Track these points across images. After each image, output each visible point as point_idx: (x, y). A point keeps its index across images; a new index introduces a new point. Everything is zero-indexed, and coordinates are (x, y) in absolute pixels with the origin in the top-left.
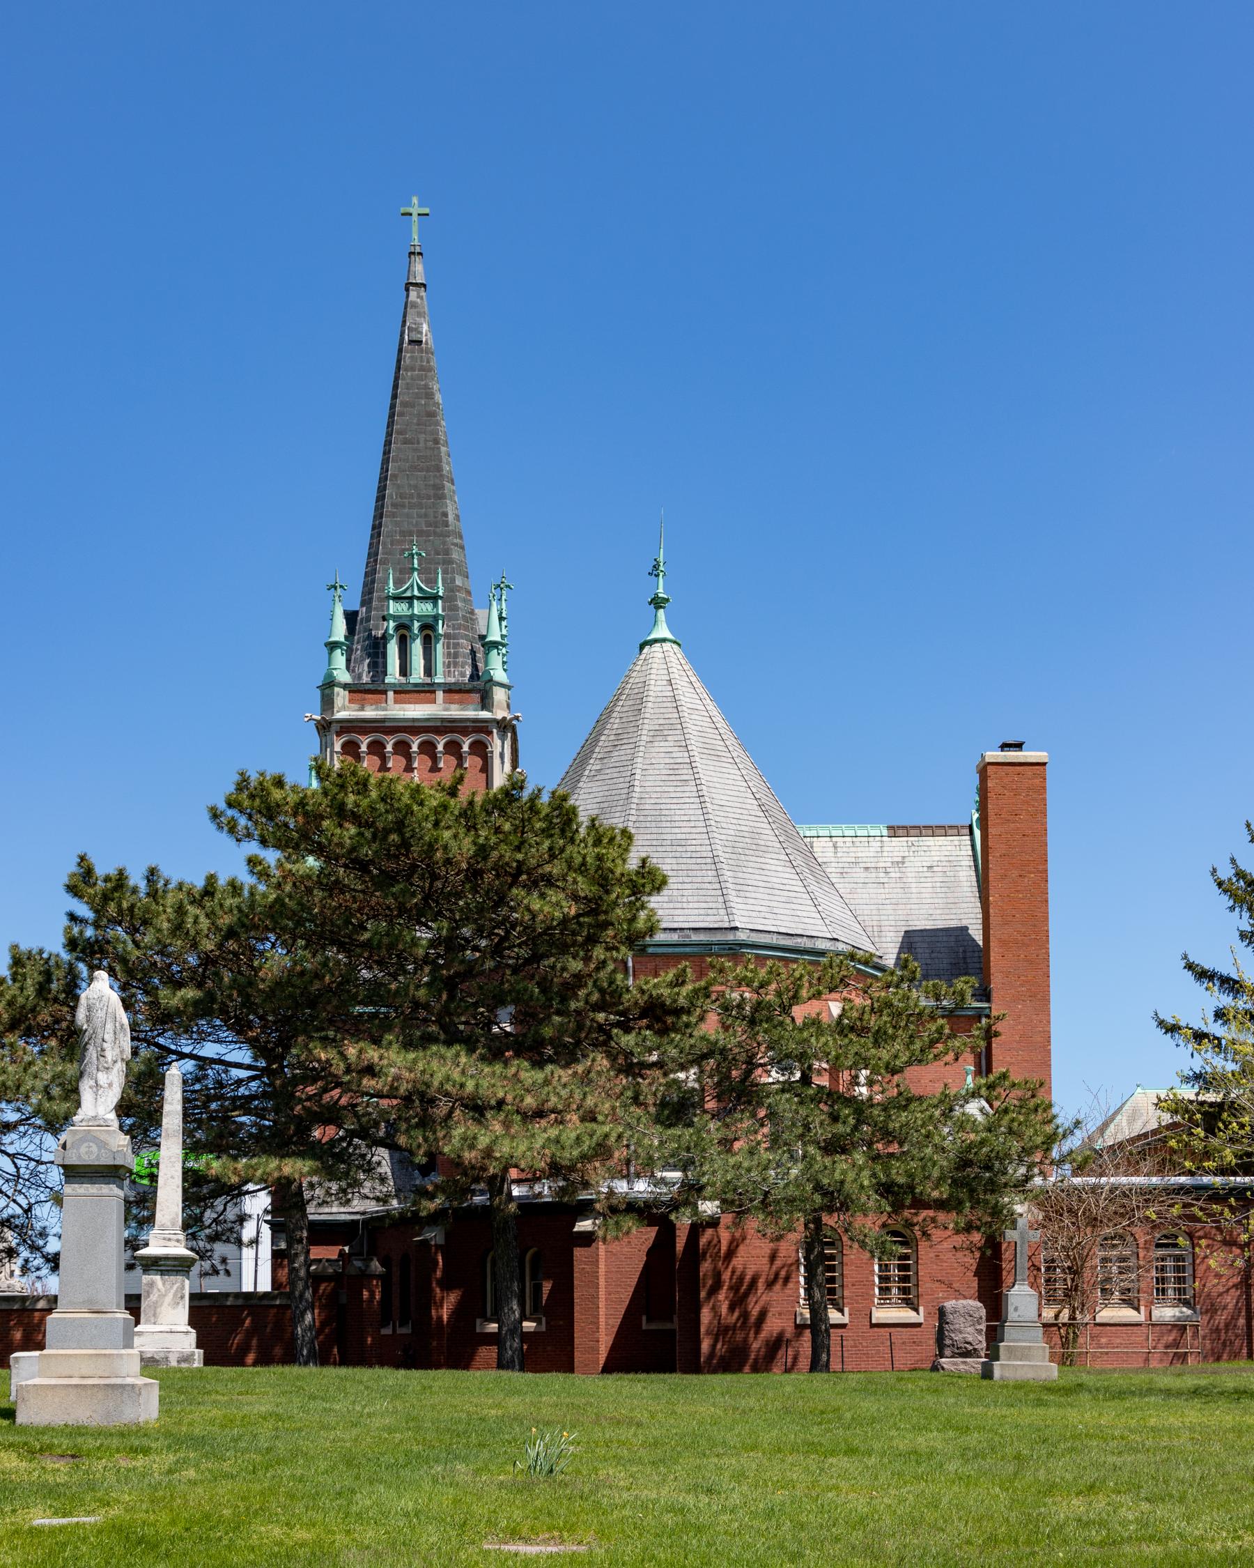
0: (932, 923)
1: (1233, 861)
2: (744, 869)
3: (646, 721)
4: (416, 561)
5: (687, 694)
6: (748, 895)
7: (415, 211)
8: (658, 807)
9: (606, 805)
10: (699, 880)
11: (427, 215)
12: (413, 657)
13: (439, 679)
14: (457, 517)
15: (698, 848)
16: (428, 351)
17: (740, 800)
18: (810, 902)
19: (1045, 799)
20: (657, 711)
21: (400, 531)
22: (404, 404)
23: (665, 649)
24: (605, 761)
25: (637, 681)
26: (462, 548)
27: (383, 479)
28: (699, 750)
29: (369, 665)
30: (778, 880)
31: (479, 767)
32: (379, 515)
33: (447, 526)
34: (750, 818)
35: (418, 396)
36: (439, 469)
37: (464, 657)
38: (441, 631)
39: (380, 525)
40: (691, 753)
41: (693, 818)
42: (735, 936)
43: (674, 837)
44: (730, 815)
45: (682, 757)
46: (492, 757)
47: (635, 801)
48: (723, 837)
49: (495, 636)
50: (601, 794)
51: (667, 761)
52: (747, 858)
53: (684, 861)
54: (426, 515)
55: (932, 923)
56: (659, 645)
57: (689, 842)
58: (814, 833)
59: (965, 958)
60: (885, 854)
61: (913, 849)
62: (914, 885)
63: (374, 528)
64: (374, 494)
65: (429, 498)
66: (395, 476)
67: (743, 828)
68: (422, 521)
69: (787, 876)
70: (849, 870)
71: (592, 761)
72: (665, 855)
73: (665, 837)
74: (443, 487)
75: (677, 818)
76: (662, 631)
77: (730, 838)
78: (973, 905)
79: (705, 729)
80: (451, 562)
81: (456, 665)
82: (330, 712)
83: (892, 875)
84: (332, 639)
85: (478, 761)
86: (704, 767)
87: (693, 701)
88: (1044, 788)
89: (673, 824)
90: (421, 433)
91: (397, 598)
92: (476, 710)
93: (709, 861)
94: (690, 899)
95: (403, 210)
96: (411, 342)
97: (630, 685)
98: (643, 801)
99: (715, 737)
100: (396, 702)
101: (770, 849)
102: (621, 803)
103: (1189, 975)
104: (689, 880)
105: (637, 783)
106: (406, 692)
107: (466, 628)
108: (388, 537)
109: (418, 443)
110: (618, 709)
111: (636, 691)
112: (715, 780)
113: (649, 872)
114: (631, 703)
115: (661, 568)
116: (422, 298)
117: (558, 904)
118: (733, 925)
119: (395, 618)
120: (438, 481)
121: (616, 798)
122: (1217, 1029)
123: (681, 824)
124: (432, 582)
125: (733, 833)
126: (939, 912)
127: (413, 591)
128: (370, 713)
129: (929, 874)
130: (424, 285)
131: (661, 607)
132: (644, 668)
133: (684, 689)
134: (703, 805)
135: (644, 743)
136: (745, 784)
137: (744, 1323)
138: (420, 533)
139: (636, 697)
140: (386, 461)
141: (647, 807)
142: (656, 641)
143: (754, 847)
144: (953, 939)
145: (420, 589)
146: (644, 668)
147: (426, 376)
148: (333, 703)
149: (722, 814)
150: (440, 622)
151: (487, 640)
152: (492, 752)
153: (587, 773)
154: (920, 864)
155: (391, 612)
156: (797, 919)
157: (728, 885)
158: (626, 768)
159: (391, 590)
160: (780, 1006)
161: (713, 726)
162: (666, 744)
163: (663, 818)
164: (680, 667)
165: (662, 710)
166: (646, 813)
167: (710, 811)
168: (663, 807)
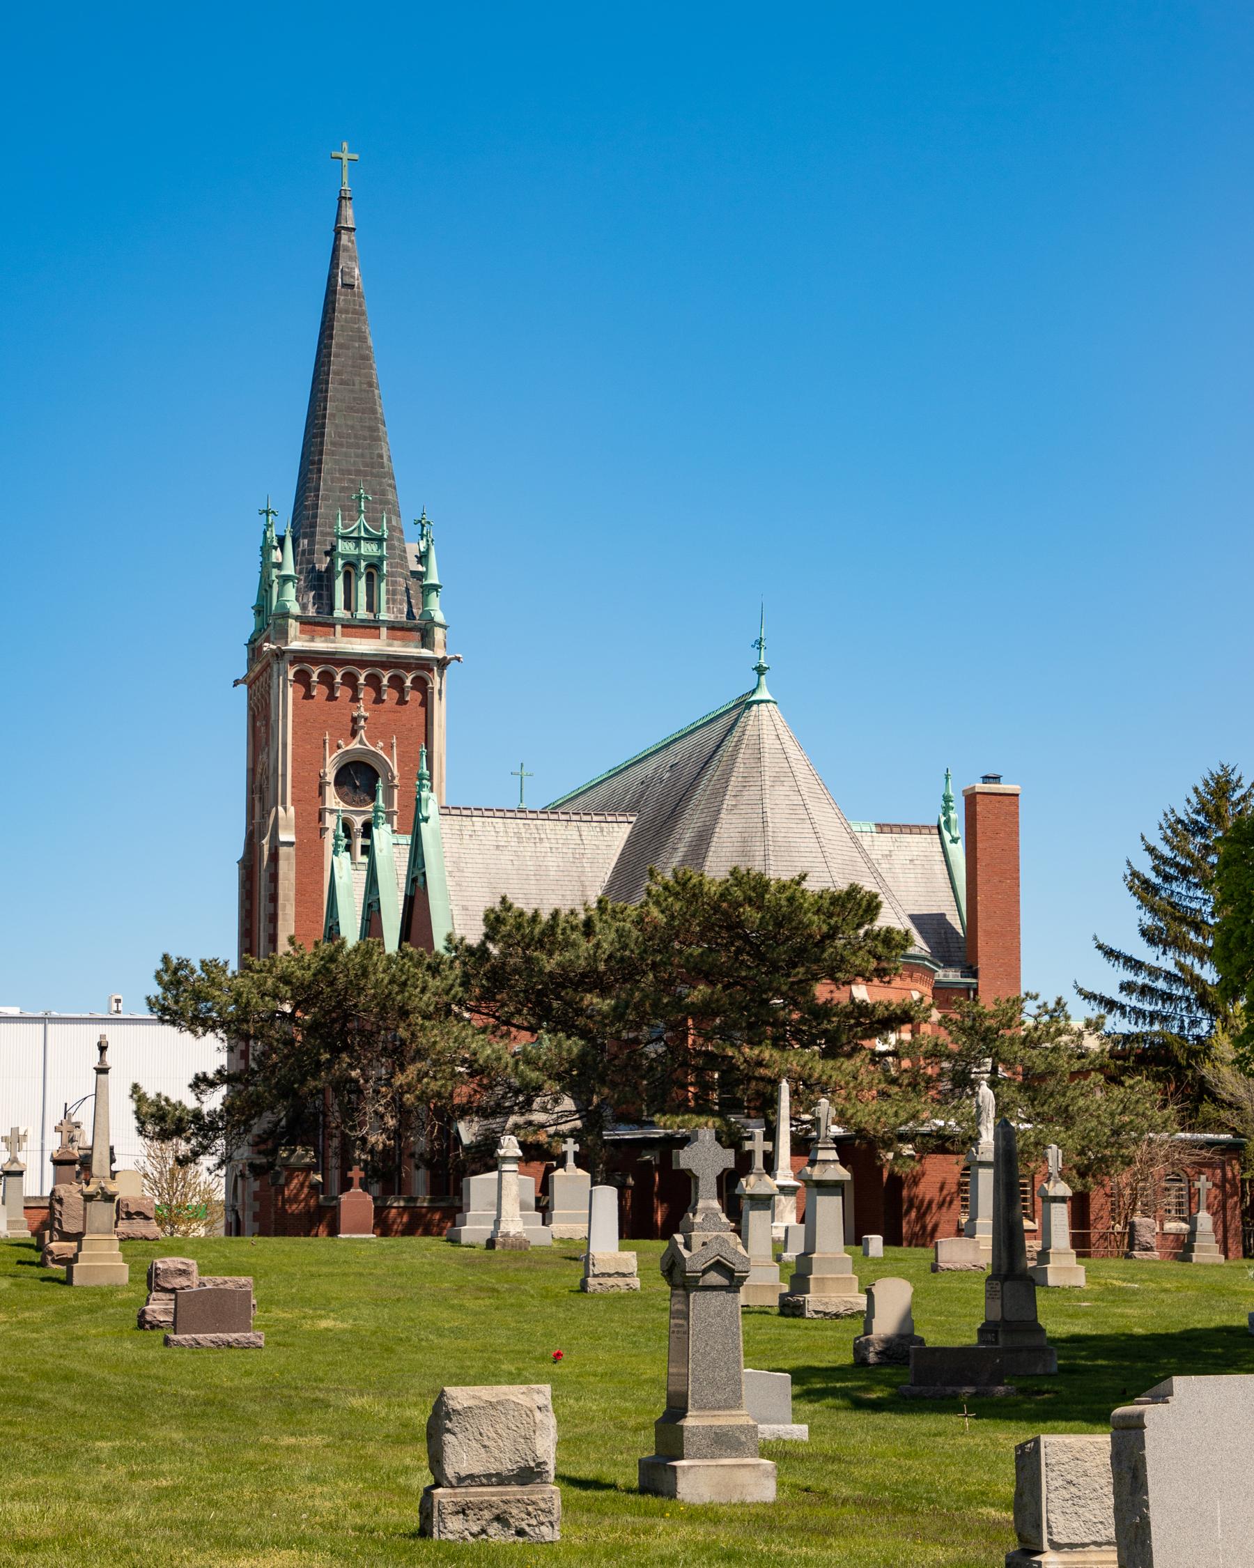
0: (917, 908)
1: (1129, 863)
9: (746, 835)
13: (384, 616)
15: (821, 874)
16: (360, 295)
19: (1018, 822)
20: (773, 760)
21: (340, 470)
26: (395, 488)
31: (419, 700)
36: (374, 411)
45: (797, 799)
46: (432, 693)
50: (740, 825)
51: (788, 802)
54: (363, 456)
55: (917, 908)
59: (946, 939)
60: (876, 848)
61: (897, 844)
62: (901, 875)
66: (333, 415)
73: (796, 864)
75: (802, 850)
78: (946, 894)
83: (883, 866)
85: (418, 696)
88: (1017, 813)
91: (345, 538)
92: (416, 647)
95: (334, 154)
100: (343, 635)
103: (1100, 953)
106: (354, 627)
114: (750, 751)
121: (754, 830)
122: (1122, 998)
124: (377, 525)
125: (840, 861)
126: (922, 899)
127: (360, 532)
128: (320, 645)
129: (911, 867)
137: (923, 1234)
144: (935, 922)
145: (366, 530)
148: (287, 633)
152: (433, 688)
154: (902, 857)
162: (784, 788)
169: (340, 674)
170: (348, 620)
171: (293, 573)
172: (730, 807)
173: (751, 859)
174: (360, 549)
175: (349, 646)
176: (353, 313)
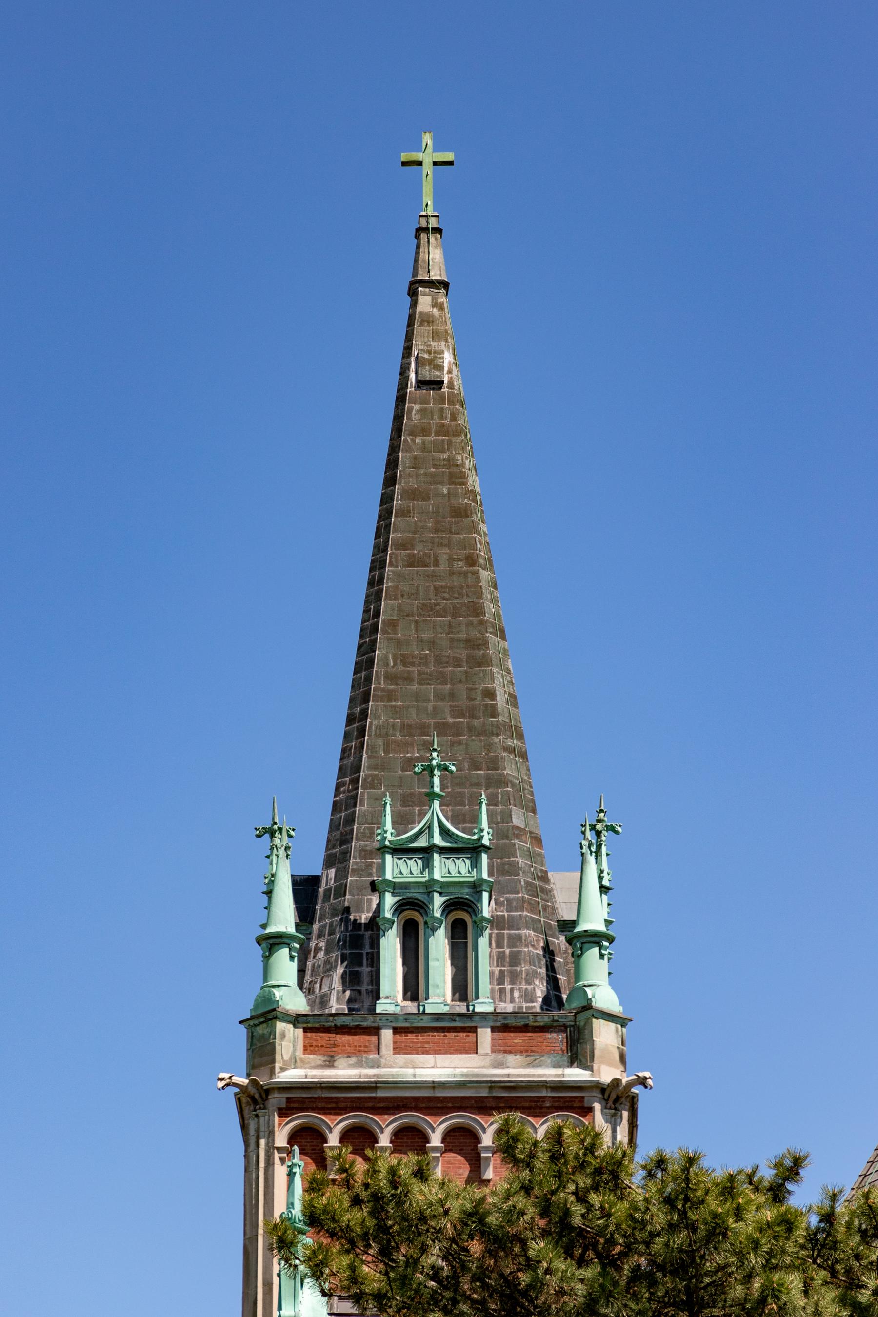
4: (437, 781)
11: (451, 163)
12: (432, 964)
13: (483, 1005)
14: (513, 700)
21: (403, 726)
22: (411, 495)
26: (523, 755)
29: (343, 977)
33: (494, 714)
35: (435, 480)
36: (477, 610)
37: (532, 963)
39: (364, 714)
54: (452, 696)
63: (350, 720)
65: (458, 663)
66: (392, 625)
68: (445, 706)
74: (485, 643)
80: (502, 782)
82: (266, 1070)
91: (401, 851)
92: (557, 1066)
95: (405, 157)
96: (421, 384)
100: (398, 1049)
107: (534, 908)
108: (379, 736)
109: (437, 563)
116: (441, 307)
119: (396, 888)
120: (474, 633)
127: (431, 836)
130: (445, 285)
138: (443, 729)
145: (444, 832)
147: (450, 443)
150: (485, 895)
151: (579, 929)
155: (389, 876)
159: (389, 836)
169: (389, 1131)
170: (408, 1016)
171: (292, 930)
174: (431, 872)
175: (410, 1071)
176: (438, 434)
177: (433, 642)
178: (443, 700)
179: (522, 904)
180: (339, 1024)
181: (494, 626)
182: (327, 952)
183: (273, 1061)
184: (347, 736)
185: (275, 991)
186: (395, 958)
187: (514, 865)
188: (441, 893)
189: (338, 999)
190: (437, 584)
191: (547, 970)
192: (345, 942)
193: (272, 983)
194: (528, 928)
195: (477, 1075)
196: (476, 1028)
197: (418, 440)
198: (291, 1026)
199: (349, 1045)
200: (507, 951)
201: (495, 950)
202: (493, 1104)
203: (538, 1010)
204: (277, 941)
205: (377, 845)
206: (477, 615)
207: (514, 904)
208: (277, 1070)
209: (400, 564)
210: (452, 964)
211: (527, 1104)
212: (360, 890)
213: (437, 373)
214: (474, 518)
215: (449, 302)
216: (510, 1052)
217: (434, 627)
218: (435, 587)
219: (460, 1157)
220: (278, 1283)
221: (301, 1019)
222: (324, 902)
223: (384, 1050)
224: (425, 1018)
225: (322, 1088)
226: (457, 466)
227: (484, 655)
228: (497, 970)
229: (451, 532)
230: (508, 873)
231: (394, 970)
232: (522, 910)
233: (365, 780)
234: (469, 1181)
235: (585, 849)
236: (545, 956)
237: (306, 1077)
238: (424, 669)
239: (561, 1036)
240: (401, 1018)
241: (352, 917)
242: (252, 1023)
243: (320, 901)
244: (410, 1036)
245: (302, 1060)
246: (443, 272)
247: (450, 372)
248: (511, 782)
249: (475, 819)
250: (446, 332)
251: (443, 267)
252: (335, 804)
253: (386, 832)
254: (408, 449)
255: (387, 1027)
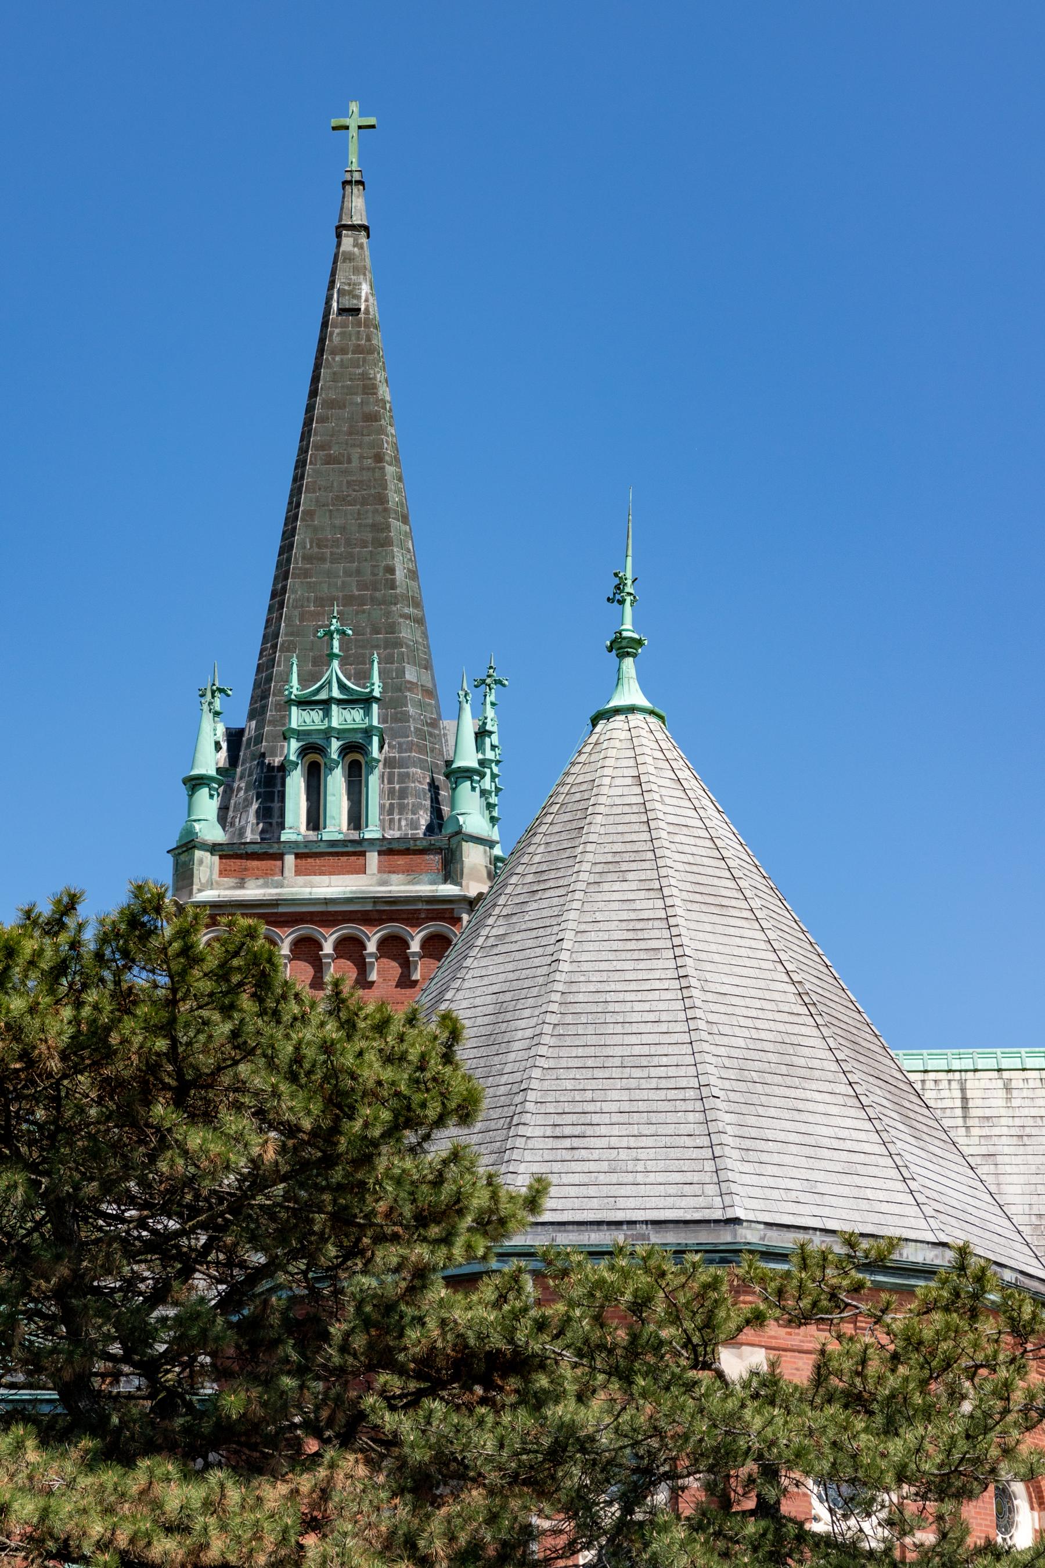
2: (761, 1111)
3: (590, 847)
4: (336, 643)
5: (667, 800)
6: (764, 1157)
7: (353, 122)
8: (602, 997)
9: (508, 996)
10: (670, 1129)
11: (373, 127)
12: (328, 798)
13: (372, 832)
14: (413, 575)
15: (672, 1071)
16: (368, 323)
17: (762, 984)
18: (895, 1173)
20: (612, 829)
21: (316, 598)
22: (330, 404)
23: (632, 724)
24: (514, 919)
25: (580, 779)
26: (420, 621)
27: (291, 519)
28: (685, 896)
29: (257, 812)
30: (830, 1132)
32: (283, 573)
33: (393, 586)
34: (778, 1016)
35: (351, 391)
36: (382, 499)
37: (417, 796)
38: (375, 754)
39: (284, 590)
40: (669, 902)
41: (664, 1017)
42: (735, 1236)
43: (627, 1051)
44: (737, 1011)
45: (652, 908)
47: (560, 987)
48: (722, 1051)
49: (468, 759)
50: (502, 977)
51: (625, 915)
52: (768, 1089)
53: (644, 1095)
54: (358, 572)
56: (622, 717)
57: (655, 1061)
58: (967, 1064)
63: (274, 595)
64: (277, 543)
65: (364, 544)
66: (310, 514)
67: (763, 1035)
68: (353, 581)
69: (849, 1123)
70: (1034, 1131)
71: (490, 921)
72: (607, 1084)
73: (609, 1051)
74: (388, 527)
76: (630, 693)
77: (735, 1053)
79: (698, 860)
80: (398, 643)
81: (402, 809)
82: (186, 891)
84: (196, 772)
86: (693, 925)
87: (679, 811)
89: (628, 1029)
90: (354, 446)
91: (304, 703)
93: (691, 1094)
94: (651, 1166)
95: (334, 122)
96: (342, 311)
97: (566, 788)
98: (574, 988)
99: (718, 873)
100: (298, 872)
101: (817, 1074)
102: (535, 991)
104: (651, 1130)
105: (564, 956)
107: (422, 750)
108: (295, 607)
109: (349, 461)
110: (543, 829)
111: (578, 796)
112: (713, 948)
113: (434, 1079)
115: (629, 589)
116: (361, 247)
117: (238, 1138)
118: (730, 1214)
119: (299, 734)
120: (379, 519)
123: (643, 1028)
124: (364, 676)
125: (741, 1043)
127: (330, 690)
128: (253, 892)
130: (366, 228)
131: (628, 654)
132: (593, 758)
133: (663, 791)
134: (686, 993)
135: (583, 886)
136: (773, 956)
138: (349, 600)
139: (576, 806)
140: (296, 492)
141: (581, 998)
142: (617, 711)
143: (784, 1069)
145: (342, 687)
146: (593, 758)
147: (364, 360)
149: (722, 1009)
150: (375, 740)
151: (454, 766)
153: (480, 941)
155: (294, 725)
156: (864, 1205)
157: (725, 1139)
158: (549, 931)
159: (295, 691)
160: (685, 1346)
161: (716, 854)
162: (625, 886)
163: (609, 1018)
164: (660, 755)
165: (620, 828)
166: (578, 1008)
167: (698, 1003)
168: (609, 997)
170: (307, 843)
172: (491, 941)
173: (503, 1048)
174: (330, 721)
175: (308, 890)
177: (344, 528)
178: (350, 576)
179: (410, 747)
180: (249, 851)
181: (396, 512)
182: (246, 792)
183: (192, 884)
184: (271, 609)
185: (196, 825)
186: (298, 794)
187: (406, 714)
188: (338, 739)
189: (252, 830)
190: (349, 478)
191: (432, 802)
192: (260, 782)
193: (193, 818)
194: (415, 767)
195: (364, 892)
196: (365, 852)
197: (338, 358)
198: (208, 854)
199: (258, 869)
200: (397, 787)
201: (387, 786)
202: (377, 917)
203: (421, 836)
204: (198, 782)
205: (285, 699)
206: (382, 503)
207: (404, 746)
208: (195, 891)
209: (319, 462)
210: (349, 799)
211: (405, 916)
212: (274, 738)
213: (355, 302)
214: (383, 422)
215: (368, 243)
216: (394, 872)
217: (346, 514)
218: (348, 482)
219: (349, 963)
220: (676, 1091)
221: (217, 848)
222: (246, 749)
223: (286, 873)
224: (322, 844)
225: (232, 906)
226: (370, 379)
227: (387, 537)
228: (387, 803)
229: (363, 435)
230: (401, 721)
231: (298, 804)
232: (411, 752)
233: (282, 645)
234: (400, 985)
235: (462, 698)
236: (430, 791)
237: (219, 896)
238: (335, 550)
239: (438, 858)
240: (302, 845)
241: (267, 761)
242: (177, 852)
243: (243, 748)
244: (309, 860)
245: (217, 883)
246: (364, 217)
247: (366, 300)
248: (406, 644)
249: (366, 676)
250: (365, 267)
251: (364, 213)
252: (259, 665)
253: (292, 687)
254: (329, 366)
255: (289, 853)
